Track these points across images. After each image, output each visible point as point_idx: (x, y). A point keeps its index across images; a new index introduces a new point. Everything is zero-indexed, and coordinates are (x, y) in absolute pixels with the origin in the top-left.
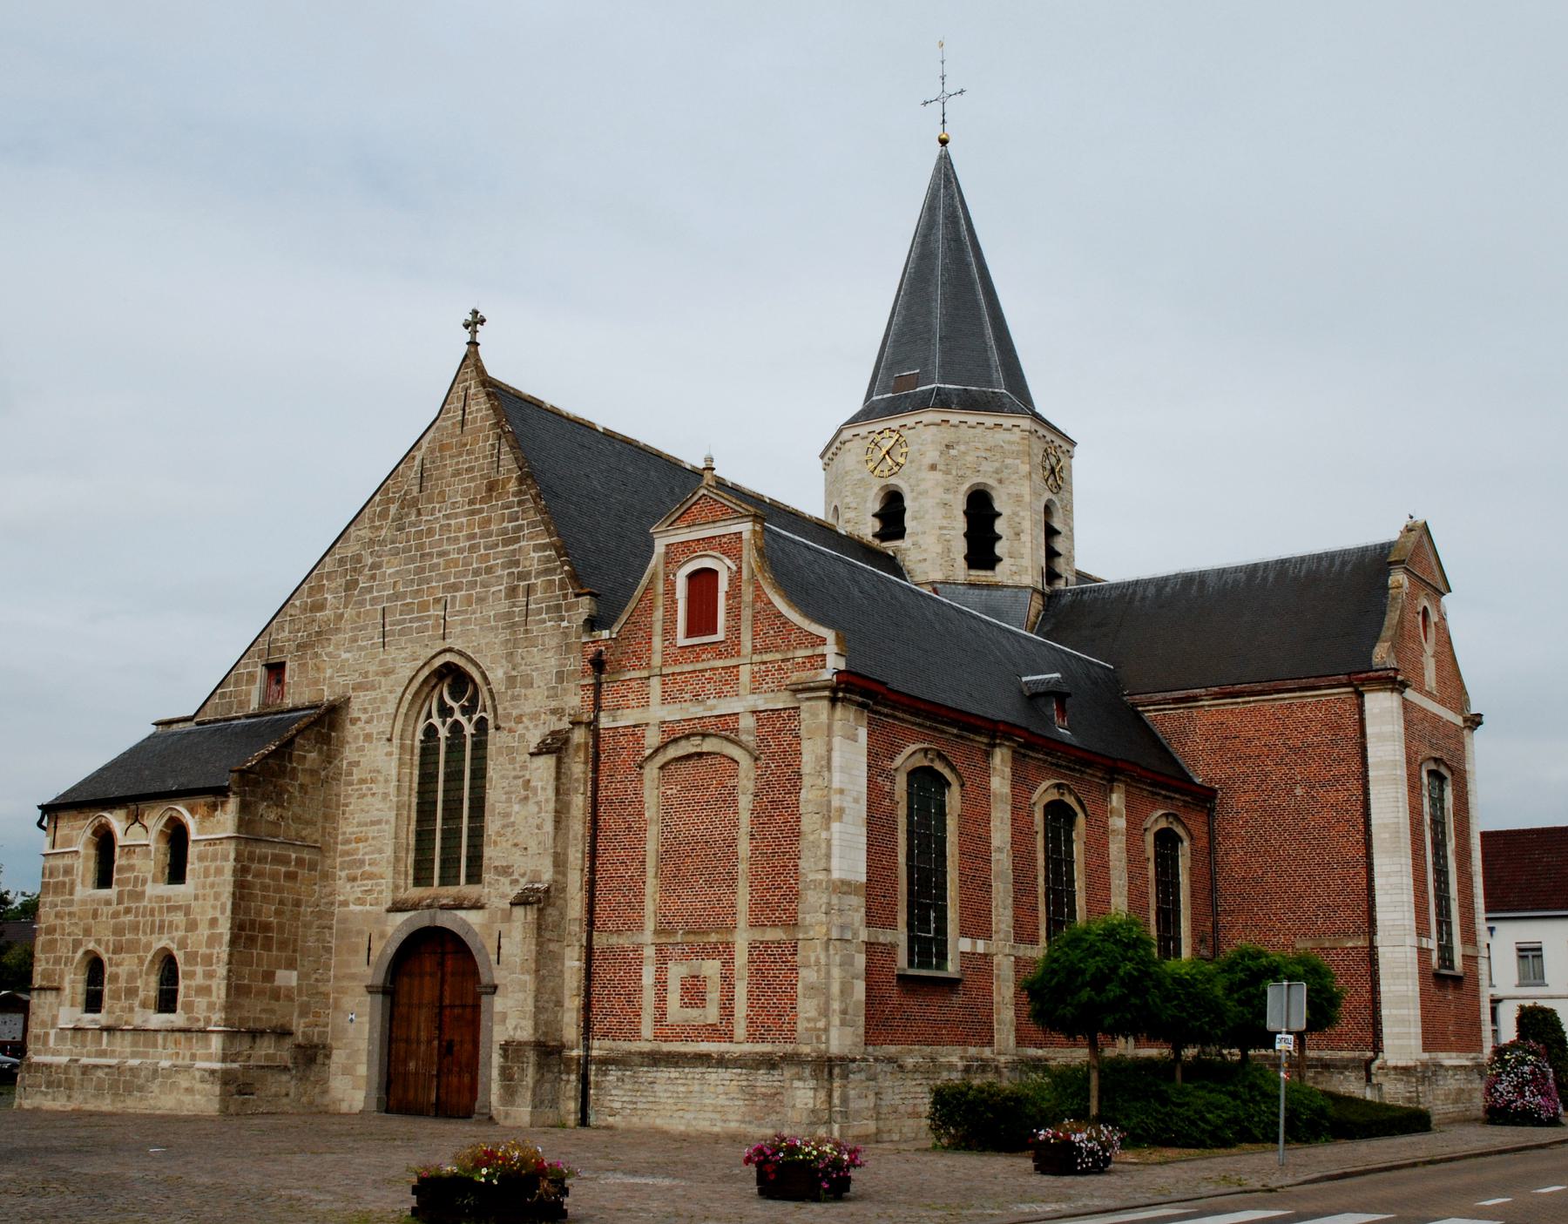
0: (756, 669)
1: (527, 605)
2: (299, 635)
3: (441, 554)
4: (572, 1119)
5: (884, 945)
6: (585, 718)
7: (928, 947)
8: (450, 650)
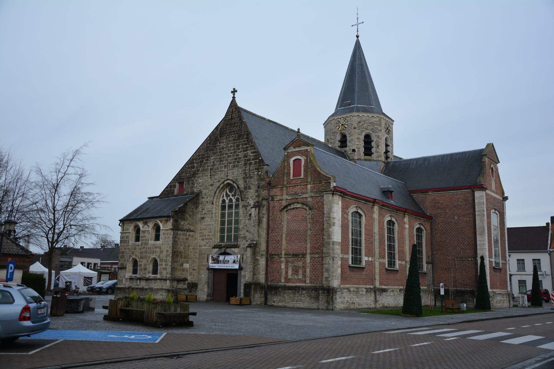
0: (312, 186)
1: (250, 168)
2: (188, 175)
3: (226, 154)
5: (345, 258)
6: (266, 198)
7: (357, 259)
8: (229, 179)
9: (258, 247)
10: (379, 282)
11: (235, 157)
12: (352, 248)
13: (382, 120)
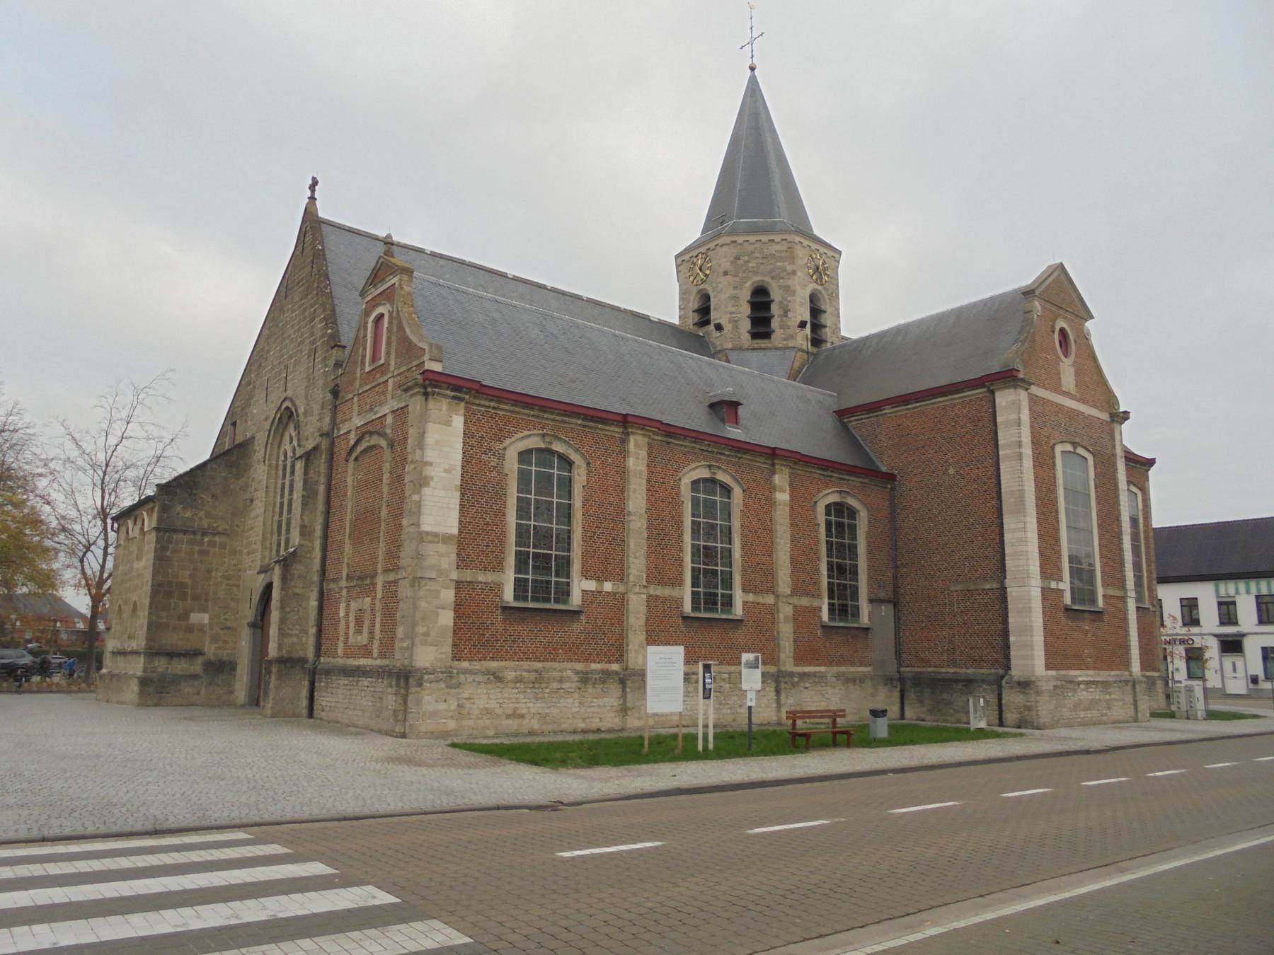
0: (396, 380)
4: (305, 712)
9: (300, 562)
13: (798, 247)
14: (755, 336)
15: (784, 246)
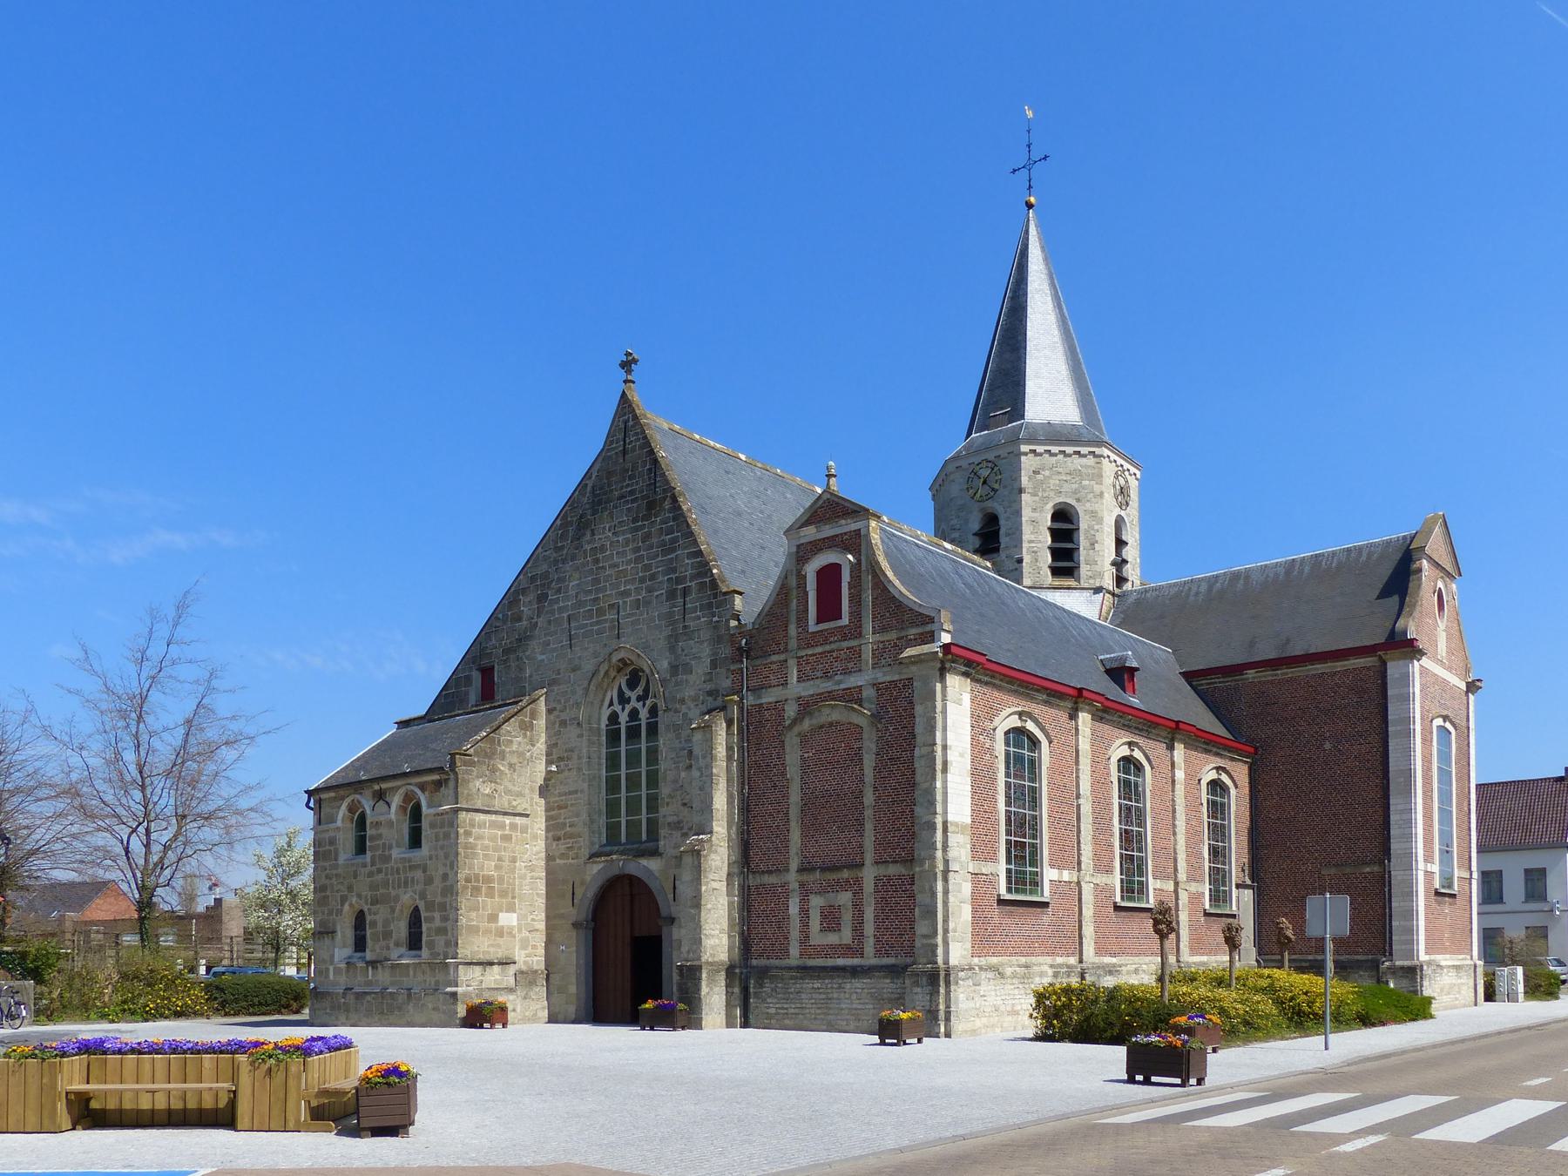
5: (986, 875)
10: (1093, 944)
11: (640, 574)
12: (1008, 842)
14: (1056, 572)
15: (1091, 461)
